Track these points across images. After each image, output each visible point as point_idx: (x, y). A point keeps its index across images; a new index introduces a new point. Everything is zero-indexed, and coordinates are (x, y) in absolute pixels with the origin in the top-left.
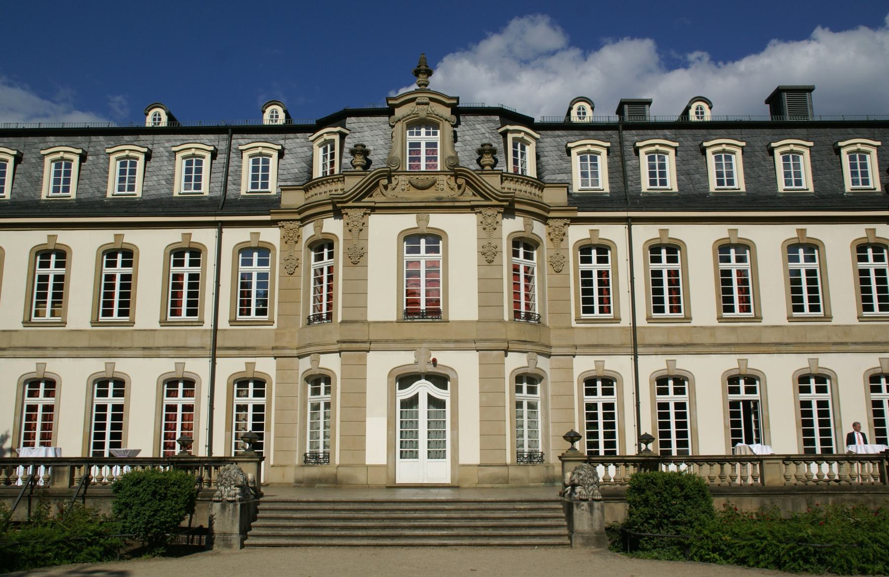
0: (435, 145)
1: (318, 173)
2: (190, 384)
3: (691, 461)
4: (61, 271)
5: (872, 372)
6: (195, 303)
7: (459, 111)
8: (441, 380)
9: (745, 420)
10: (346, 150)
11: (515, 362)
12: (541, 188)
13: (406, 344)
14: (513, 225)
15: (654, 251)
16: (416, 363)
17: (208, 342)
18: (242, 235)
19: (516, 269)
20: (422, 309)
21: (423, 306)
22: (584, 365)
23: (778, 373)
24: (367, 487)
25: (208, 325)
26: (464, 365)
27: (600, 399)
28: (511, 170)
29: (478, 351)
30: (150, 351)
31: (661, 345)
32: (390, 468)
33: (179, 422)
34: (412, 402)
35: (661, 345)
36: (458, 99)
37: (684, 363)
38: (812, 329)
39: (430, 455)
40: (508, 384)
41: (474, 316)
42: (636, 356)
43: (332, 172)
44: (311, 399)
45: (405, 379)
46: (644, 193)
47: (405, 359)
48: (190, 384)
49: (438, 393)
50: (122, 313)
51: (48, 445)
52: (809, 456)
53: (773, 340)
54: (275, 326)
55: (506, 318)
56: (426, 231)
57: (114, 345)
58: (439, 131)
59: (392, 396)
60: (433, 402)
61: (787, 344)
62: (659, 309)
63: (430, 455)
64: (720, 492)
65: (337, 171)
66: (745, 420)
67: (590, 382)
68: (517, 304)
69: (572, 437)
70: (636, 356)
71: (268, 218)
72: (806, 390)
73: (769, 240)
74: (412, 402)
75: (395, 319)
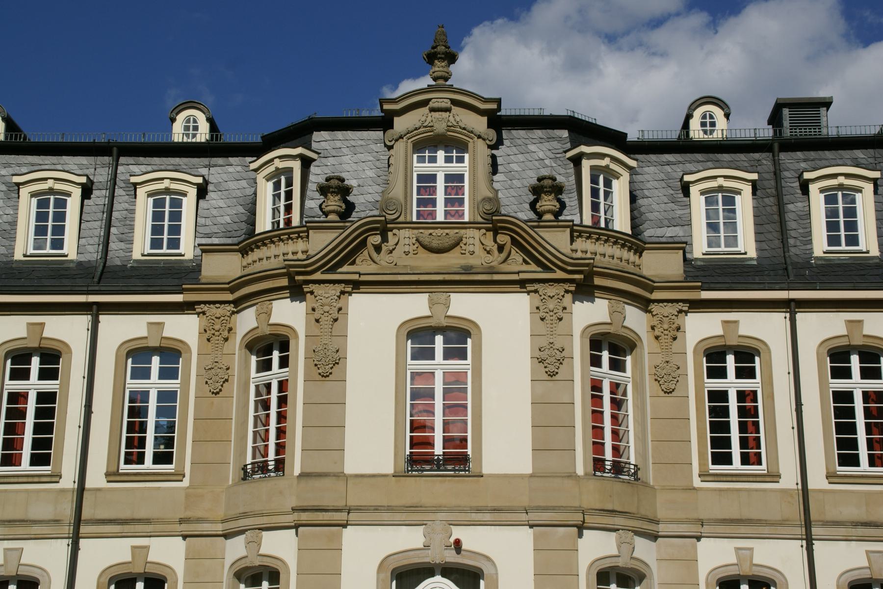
0: (460, 178)
1: (264, 223)
7: (500, 122)
12: (639, 251)
14: (592, 313)
16: (427, 547)
17: (67, 510)
18: (135, 327)
19: (596, 386)
20: (436, 454)
25: (68, 480)
29: (531, 526)
35: (856, 524)
36: (498, 101)
41: (525, 467)
42: (809, 542)
43: (288, 222)
46: (817, 258)
47: (407, 540)
54: (186, 482)
55: (580, 471)
56: (445, 323)
58: (467, 156)
65: (296, 221)
68: (598, 447)
70: (809, 542)
75: (390, 470)
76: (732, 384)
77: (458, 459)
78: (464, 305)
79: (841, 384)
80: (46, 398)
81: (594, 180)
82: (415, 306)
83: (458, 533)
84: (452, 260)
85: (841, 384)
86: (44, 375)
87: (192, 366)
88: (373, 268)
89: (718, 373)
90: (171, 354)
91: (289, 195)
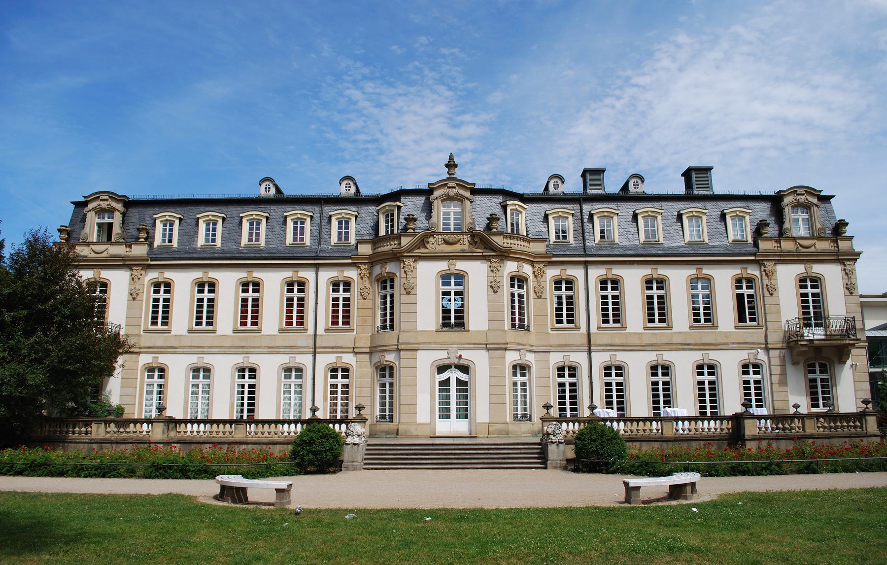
1: (382, 232)
2: (299, 370)
3: (257, 422)
4: (256, 295)
5: (743, 362)
6: (302, 317)
7: (476, 192)
8: (465, 369)
9: (662, 394)
10: (402, 217)
11: (512, 357)
12: (529, 242)
13: (443, 346)
14: (511, 267)
15: (603, 283)
16: (449, 358)
17: (311, 343)
18: (333, 274)
19: (513, 295)
20: (453, 320)
21: (453, 321)
22: (556, 358)
23: (684, 365)
24: (418, 437)
25: (311, 332)
26: (479, 360)
27: (567, 380)
28: (509, 230)
29: (488, 349)
30: (273, 350)
31: (606, 345)
32: (432, 424)
33: (820, 390)
34: (447, 382)
35: (606, 345)
36: (474, 184)
37: (622, 357)
38: (660, 336)
39: (458, 417)
40: (508, 370)
41: (485, 327)
42: (590, 352)
43: (392, 231)
44: (192, 381)
45: (442, 369)
47: (441, 356)
48: (299, 370)
49: (463, 377)
50: (253, 324)
51: (761, 406)
52: (703, 416)
53: (680, 342)
54: (355, 333)
55: (506, 329)
56: (455, 272)
57: (248, 345)
59: (433, 379)
60: (459, 382)
61: (689, 344)
62: (606, 321)
63: (458, 417)
64: (630, 440)
65: (396, 231)
66: (662, 394)
67: (561, 369)
68: (513, 319)
69: (547, 407)
70: (590, 352)
71: (350, 261)
72: (655, 374)
73: (228, 282)
74: (447, 382)
75: (434, 329)
76: (655, 292)
77: (461, 323)
78: (818, 269)
79: (649, 292)
80: (301, 300)
81: (512, 214)
82: (442, 266)
83: (460, 352)
84: (457, 247)
85: (649, 292)
86: (210, 291)
87: (355, 287)
88: (426, 251)
89: (605, 289)
90: (347, 285)
91: (392, 220)
